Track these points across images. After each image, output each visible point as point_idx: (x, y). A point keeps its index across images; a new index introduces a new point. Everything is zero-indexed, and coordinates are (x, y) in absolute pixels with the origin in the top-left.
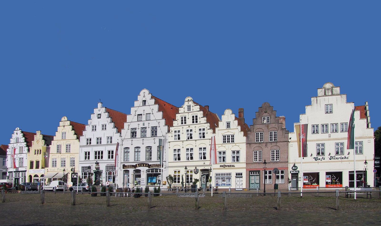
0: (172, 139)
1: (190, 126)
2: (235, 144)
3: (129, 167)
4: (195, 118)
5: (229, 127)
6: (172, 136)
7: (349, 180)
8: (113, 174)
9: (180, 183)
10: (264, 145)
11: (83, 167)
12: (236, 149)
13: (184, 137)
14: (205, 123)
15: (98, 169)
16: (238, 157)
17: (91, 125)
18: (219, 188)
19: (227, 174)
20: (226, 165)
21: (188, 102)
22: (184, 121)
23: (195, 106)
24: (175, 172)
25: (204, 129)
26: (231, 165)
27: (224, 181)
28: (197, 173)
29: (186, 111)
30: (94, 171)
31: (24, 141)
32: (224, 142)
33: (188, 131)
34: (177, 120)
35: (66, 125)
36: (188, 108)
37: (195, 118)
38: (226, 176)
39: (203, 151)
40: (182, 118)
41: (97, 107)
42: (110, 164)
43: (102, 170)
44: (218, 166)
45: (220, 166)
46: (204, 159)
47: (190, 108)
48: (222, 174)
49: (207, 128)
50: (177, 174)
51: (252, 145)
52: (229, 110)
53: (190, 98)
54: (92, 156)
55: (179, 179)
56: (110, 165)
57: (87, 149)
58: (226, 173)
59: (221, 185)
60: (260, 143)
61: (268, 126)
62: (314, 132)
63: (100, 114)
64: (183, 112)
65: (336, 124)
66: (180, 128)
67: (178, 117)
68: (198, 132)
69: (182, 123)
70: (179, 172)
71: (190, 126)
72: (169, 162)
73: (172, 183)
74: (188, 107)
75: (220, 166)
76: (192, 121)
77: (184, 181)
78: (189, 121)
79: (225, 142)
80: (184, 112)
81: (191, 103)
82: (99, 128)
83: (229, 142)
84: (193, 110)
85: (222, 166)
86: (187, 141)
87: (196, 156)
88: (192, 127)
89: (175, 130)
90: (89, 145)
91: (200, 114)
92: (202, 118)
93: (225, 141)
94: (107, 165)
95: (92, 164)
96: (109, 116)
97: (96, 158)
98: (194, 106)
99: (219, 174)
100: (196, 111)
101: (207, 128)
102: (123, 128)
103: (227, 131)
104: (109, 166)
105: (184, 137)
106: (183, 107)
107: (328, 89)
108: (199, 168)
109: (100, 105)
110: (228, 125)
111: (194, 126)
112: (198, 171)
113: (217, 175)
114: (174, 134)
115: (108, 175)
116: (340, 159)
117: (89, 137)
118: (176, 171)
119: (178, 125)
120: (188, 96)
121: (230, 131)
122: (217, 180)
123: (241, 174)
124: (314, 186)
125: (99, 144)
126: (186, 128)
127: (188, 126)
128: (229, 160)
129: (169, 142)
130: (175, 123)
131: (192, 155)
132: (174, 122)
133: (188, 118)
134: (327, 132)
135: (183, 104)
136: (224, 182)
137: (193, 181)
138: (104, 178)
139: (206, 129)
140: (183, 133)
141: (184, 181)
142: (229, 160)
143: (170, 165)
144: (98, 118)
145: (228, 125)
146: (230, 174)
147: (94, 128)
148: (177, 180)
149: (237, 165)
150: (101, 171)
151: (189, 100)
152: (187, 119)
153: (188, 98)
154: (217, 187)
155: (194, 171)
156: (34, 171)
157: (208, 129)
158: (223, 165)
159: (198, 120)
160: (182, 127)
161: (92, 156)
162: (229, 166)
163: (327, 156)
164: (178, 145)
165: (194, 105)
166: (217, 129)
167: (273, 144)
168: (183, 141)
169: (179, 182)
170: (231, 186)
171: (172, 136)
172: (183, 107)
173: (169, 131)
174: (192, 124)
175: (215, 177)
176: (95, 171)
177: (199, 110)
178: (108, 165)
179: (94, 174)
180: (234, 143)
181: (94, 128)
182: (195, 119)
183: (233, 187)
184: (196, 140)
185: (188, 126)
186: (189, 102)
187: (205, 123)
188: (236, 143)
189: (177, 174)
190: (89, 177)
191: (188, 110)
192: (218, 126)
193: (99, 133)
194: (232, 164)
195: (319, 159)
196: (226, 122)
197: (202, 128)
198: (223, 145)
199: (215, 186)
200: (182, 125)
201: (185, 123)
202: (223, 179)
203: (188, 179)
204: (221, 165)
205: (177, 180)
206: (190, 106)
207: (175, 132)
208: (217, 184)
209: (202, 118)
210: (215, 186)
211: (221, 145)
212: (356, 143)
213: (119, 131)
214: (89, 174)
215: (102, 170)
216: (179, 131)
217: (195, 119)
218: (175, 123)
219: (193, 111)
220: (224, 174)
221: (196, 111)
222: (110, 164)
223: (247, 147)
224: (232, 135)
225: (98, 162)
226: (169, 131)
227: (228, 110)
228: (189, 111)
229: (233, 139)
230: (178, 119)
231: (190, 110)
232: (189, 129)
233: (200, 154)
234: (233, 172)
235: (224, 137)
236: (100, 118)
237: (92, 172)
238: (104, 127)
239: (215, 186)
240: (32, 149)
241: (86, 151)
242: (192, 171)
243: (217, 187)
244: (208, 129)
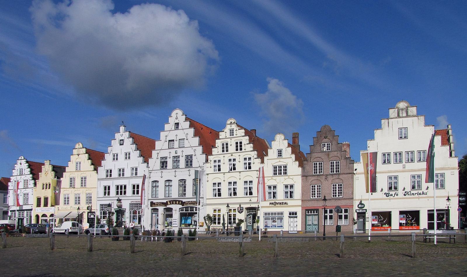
0: (211, 170)
2: (287, 177)
3: (157, 204)
4: (239, 145)
5: (281, 156)
6: (211, 167)
8: (139, 214)
9: (221, 225)
10: (324, 177)
11: (101, 205)
12: (289, 182)
13: (225, 168)
14: (251, 151)
15: (120, 207)
16: (274, 193)
17: (111, 154)
18: (269, 230)
19: (278, 214)
20: (277, 202)
22: (225, 148)
23: (239, 129)
25: (250, 159)
26: (283, 203)
27: (275, 222)
28: (242, 212)
29: (228, 136)
30: (115, 210)
31: (29, 173)
32: (275, 174)
33: (230, 160)
34: (217, 148)
35: (81, 153)
36: (230, 133)
37: (239, 145)
38: (270, 216)
40: (223, 144)
41: (118, 131)
42: (134, 200)
43: (125, 209)
44: (267, 203)
45: (270, 203)
47: (233, 133)
48: (272, 214)
49: (253, 157)
50: (217, 213)
51: (309, 178)
52: (281, 135)
54: (113, 191)
55: (219, 219)
56: (134, 203)
57: (107, 183)
59: (271, 227)
60: (318, 175)
61: (328, 155)
62: (385, 162)
63: (123, 140)
65: (412, 152)
66: (221, 157)
67: (219, 143)
68: (243, 162)
69: (223, 151)
70: (219, 210)
71: (233, 154)
72: (207, 198)
74: (230, 131)
75: (270, 203)
76: (235, 148)
77: (226, 222)
78: (232, 148)
79: (276, 174)
80: (226, 138)
81: (234, 127)
82: (121, 157)
83: (281, 174)
84: (236, 135)
85: (272, 204)
87: (225, 192)
88: (236, 156)
89: (215, 159)
90: (109, 177)
92: (247, 144)
93: (276, 173)
94: (131, 203)
95: (113, 201)
96: (134, 143)
97: (117, 193)
99: (269, 214)
101: (253, 157)
102: (151, 156)
103: (278, 160)
104: (133, 203)
105: (225, 168)
106: (225, 132)
107: (402, 109)
108: (244, 206)
109: (122, 129)
110: (280, 153)
111: (238, 154)
112: (243, 210)
113: (266, 214)
115: (132, 215)
116: (416, 194)
117: (109, 168)
118: (216, 210)
119: (219, 153)
121: (281, 160)
122: (266, 221)
123: (296, 214)
124: (384, 228)
125: (121, 176)
126: (228, 157)
128: (281, 196)
132: (213, 149)
133: (231, 145)
134: (401, 161)
135: (224, 127)
136: (274, 224)
137: (237, 221)
138: (127, 218)
139: (252, 159)
140: (224, 163)
141: (226, 222)
142: (281, 196)
144: (120, 145)
145: (280, 153)
146: (282, 213)
147: (115, 157)
148: (217, 221)
149: (290, 202)
150: (124, 210)
151: (231, 123)
152: (229, 146)
153: (231, 120)
154: (266, 229)
155: (238, 210)
156: (42, 210)
157: (255, 158)
158: (273, 202)
159: (243, 147)
161: (113, 191)
162: (280, 204)
163: (400, 192)
164: (218, 178)
165: (238, 129)
166: (266, 158)
167: (335, 177)
168: (224, 173)
169: (219, 223)
170: (283, 227)
171: (211, 167)
172: (225, 132)
173: (207, 161)
175: (264, 217)
176: (116, 210)
178: (133, 203)
179: (116, 213)
180: (287, 176)
181: (115, 157)
183: (286, 229)
184: (240, 172)
185: (230, 155)
187: (251, 151)
188: (289, 176)
189: (217, 213)
190: (109, 216)
191: (231, 135)
192: (267, 155)
193: (122, 163)
194: (284, 201)
195: (391, 195)
196: (277, 150)
198: (273, 178)
199: (264, 228)
200: (223, 153)
201: (227, 151)
202: (273, 219)
204: (271, 202)
205: (217, 221)
206: (233, 130)
207: (215, 161)
208: (266, 226)
209: (247, 144)
210: (264, 228)
211: (271, 178)
212: (437, 176)
213: (146, 161)
214: (110, 213)
215: (125, 209)
216: (219, 161)
219: (237, 136)
220: (275, 214)
222: (134, 200)
223: (302, 180)
224: (285, 165)
225: (120, 198)
226: (207, 161)
227: (279, 135)
228: (232, 136)
229: (286, 170)
231: (233, 135)
232: (232, 158)
233: (246, 188)
234: (286, 211)
235: (275, 167)
236: (123, 144)
237: (113, 211)
238: (128, 156)
239: (263, 228)
240: (40, 183)
241: (105, 185)
242: (235, 210)
243: (266, 229)
244: (255, 158)
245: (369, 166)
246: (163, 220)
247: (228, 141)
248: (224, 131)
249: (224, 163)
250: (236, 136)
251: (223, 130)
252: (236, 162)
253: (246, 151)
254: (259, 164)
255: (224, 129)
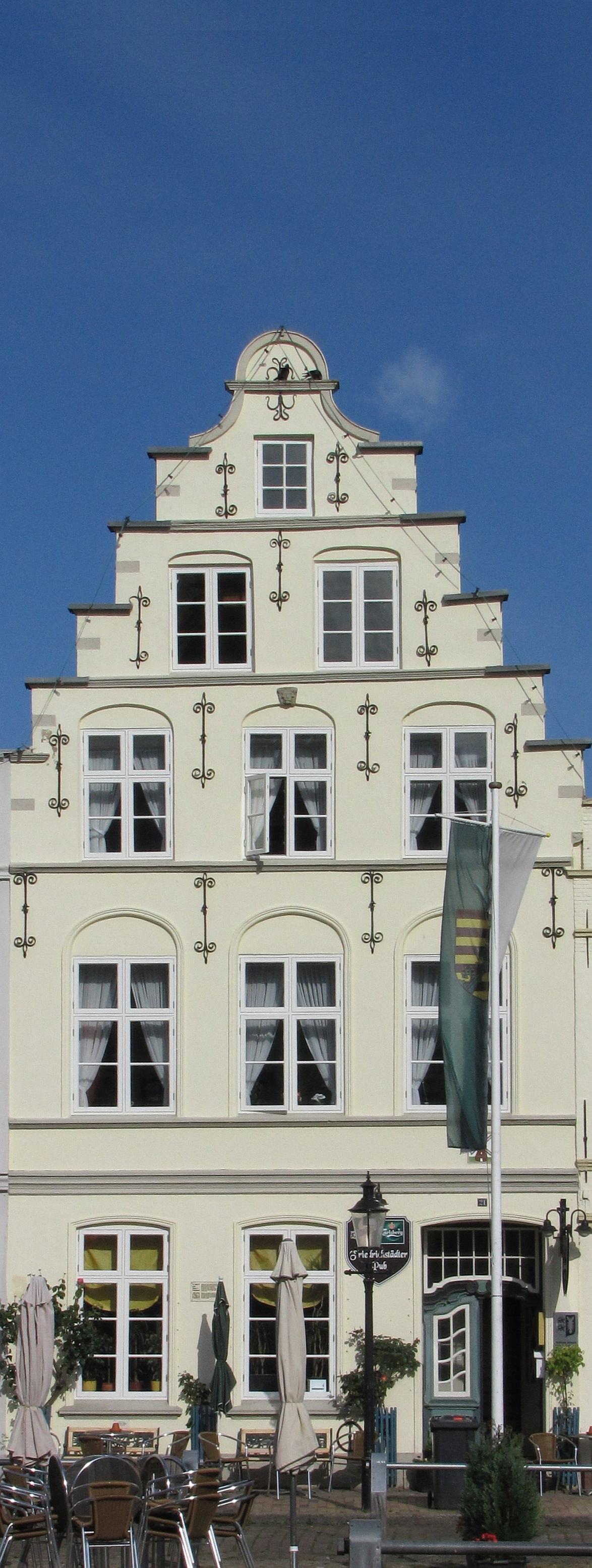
0: (72, 835)
1: (304, 694)
4: (212, 603)
6: (59, 805)
7: (118, 1287)
9: (169, 1393)
13: (214, 816)
14: (491, 673)
21: (274, 399)
22: (214, 620)
23: (363, 450)
24: (100, 1245)
25: (472, 746)
28: (396, 1266)
29: (250, 503)
33: (265, 747)
34: (125, 611)
36: (271, 476)
37: (212, 603)
39: (133, 1005)
40: (191, 586)
46: (305, 1098)
47: (298, 476)
49: (512, 728)
50: (125, 1275)
53: (301, 359)
55: (147, 1335)
58: (505, 1257)
64: (214, 518)
67: (147, 566)
68: (400, 770)
69: (191, 651)
70: (149, 1245)
71: (304, 694)
72: (17, 1115)
73: (59, 1389)
74: (271, 454)
76: (319, 632)
78: (286, 635)
80: (226, 520)
81: (308, 414)
84: (339, 500)
86: (260, 868)
87: (209, 1061)
88: (330, 708)
89: (104, 725)
91: (429, 560)
92: (449, 601)
98: (351, 450)
100: (385, 521)
101: (512, 728)
105: (214, 816)
106: (216, 459)
111: (357, 693)
112: (406, 1248)
114: (81, 774)
118: (109, 1243)
119: (147, 671)
120: (282, 324)
126: (243, 710)
127: (270, 694)
129: (25, 874)
130: (95, 643)
131: (154, 1044)
132: (89, 627)
133: (280, 599)
135: (214, 406)
137: (344, 1359)
139: (500, 748)
140: (203, 776)
143: (28, 1154)
148: (122, 1356)
151: (284, 372)
153: (279, 352)
155: (352, 1244)
157: (532, 747)
159: (408, 630)
160: (194, 695)
165: (350, 446)
168: (205, 874)
169: (145, 1375)
171: (59, 805)
172: (216, 459)
174: (323, 666)
177: (409, 504)
182: (362, 620)
184: (372, 872)
185: (270, 694)
186: (287, 399)
187: (491, 673)
189: (125, 1275)
191: (271, 500)
197: (448, 725)
201: (233, 650)
203: (264, 1337)
205: (122, 1356)
206: (297, 454)
207: (104, 748)
209: (449, 601)
216: (151, 748)
217: (362, 620)
218: (95, 643)
219: (346, 511)
221: (385, 521)
228: (284, 513)
230: (144, 601)
231: (298, 500)
232: (288, 725)
242: (321, 1243)
244: (532, 747)
245: (154, 1532)
246: (95, 1172)
247: (257, 549)
248: (203, 454)
249: (203, 776)
250: (326, 510)
251: (194, 442)
252: (175, 775)
253: (437, 663)
254: (568, 801)
255: (209, 437)
